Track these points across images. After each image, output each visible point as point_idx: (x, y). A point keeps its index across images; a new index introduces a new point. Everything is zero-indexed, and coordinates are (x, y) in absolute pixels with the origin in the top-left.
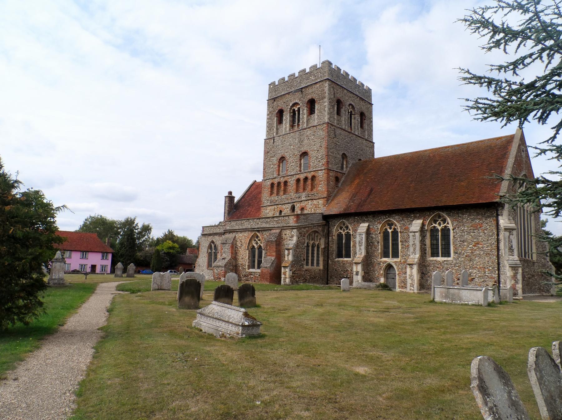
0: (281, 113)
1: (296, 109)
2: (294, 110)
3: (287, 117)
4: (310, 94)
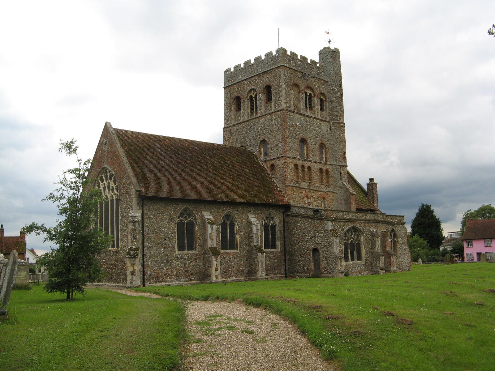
0: (238, 99)
1: (253, 96)
2: (251, 97)
3: (245, 104)
4: (268, 79)
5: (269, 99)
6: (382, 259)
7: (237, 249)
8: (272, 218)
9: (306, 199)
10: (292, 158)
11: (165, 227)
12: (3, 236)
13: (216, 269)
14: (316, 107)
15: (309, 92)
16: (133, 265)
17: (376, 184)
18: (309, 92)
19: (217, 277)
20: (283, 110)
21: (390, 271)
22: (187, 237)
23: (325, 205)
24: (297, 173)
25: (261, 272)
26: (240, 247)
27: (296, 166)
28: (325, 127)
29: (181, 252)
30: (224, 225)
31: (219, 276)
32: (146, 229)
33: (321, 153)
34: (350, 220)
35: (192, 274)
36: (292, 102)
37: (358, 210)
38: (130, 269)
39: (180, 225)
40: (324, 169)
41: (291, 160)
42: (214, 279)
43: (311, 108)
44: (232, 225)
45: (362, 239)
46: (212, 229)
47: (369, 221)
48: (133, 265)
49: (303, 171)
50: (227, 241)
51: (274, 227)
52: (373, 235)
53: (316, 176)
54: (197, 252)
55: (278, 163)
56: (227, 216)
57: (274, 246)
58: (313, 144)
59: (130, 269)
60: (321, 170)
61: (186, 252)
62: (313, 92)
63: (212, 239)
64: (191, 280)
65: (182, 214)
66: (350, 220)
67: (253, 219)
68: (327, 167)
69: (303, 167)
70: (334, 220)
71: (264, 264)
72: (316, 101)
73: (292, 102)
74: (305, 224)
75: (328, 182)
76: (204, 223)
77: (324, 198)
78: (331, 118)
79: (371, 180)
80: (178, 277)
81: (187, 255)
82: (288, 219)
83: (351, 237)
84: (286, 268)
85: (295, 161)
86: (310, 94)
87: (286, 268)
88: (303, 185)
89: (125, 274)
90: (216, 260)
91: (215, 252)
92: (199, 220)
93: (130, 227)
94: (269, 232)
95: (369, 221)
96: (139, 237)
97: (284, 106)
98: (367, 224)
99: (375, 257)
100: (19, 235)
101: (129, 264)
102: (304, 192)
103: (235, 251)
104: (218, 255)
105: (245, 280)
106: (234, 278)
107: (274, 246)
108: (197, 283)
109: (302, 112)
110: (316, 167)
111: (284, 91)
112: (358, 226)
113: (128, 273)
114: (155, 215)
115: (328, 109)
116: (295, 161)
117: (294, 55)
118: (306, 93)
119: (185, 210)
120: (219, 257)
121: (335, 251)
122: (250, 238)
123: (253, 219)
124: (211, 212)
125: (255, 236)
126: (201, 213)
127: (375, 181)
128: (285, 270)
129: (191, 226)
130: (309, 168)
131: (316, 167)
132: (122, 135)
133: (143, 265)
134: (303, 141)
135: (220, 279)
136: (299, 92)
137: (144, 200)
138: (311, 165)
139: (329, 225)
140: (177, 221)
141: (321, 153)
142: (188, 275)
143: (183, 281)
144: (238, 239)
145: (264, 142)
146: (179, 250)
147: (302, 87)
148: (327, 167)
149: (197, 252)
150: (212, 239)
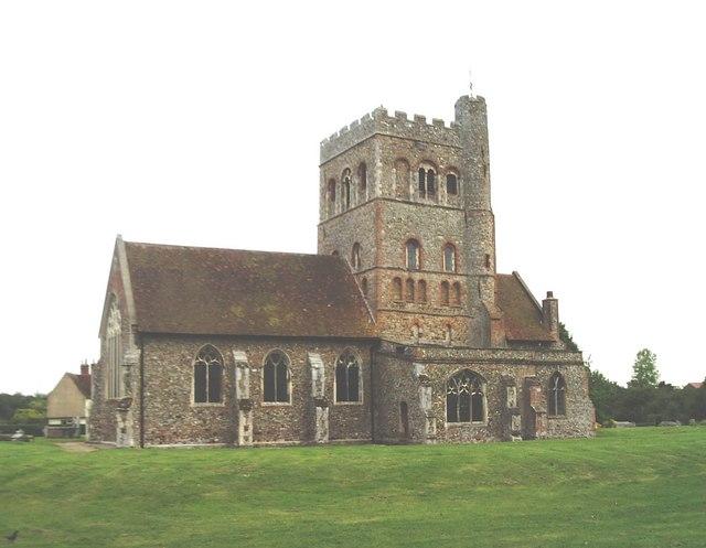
4: (363, 154)
5: (363, 185)
6: (517, 420)
7: (288, 401)
8: (352, 358)
9: (414, 329)
10: (389, 268)
11: (175, 371)
12: (488, 261)
13: (246, 429)
14: (440, 189)
15: (427, 168)
16: (124, 420)
17: (556, 300)
18: (427, 168)
19: (246, 439)
20: (377, 198)
21: (534, 438)
22: (212, 384)
23: (450, 335)
24: (400, 289)
25: (321, 434)
26: (295, 399)
27: (397, 280)
28: (455, 218)
29: (200, 404)
30: (268, 369)
31: (251, 438)
32: (147, 375)
33: (448, 257)
34: (460, 361)
35: (215, 434)
36: (394, 187)
37: (513, 344)
38: (121, 425)
39: (200, 369)
40: (451, 281)
41: (389, 272)
42: (242, 442)
43: (432, 191)
44: (283, 369)
45: (484, 388)
46: (243, 374)
47: (498, 361)
48: (124, 420)
49: (410, 289)
50: (274, 387)
51: (355, 369)
52: (507, 383)
53: (434, 294)
54: (223, 405)
55: (371, 275)
56: (275, 356)
57: (355, 398)
58: (431, 246)
59: (121, 425)
60: (445, 284)
61: (208, 404)
62: (436, 168)
63: (243, 388)
64: (214, 442)
65: (201, 355)
66: (460, 361)
67: (316, 360)
68: (458, 279)
69: (410, 281)
70: (424, 362)
71: (327, 423)
72: (441, 179)
73: (394, 187)
74: (395, 366)
75: (459, 302)
76: (233, 365)
77: (449, 326)
78: (467, 204)
79: (550, 294)
80: (193, 437)
81: (208, 408)
82: (379, 359)
83: (464, 387)
84: (373, 428)
85: (396, 274)
86: (430, 171)
87: (373, 428)
88: (409, 307)
89: (115, 430)
90: (247, 417)
91: (246, 405)
92: (226, 362)
93: (124, 371)
94: (346, 381)
95: (498, 361)
96: (135, 384)
97: (379, 193)
98: (494, 366)
99: (504, 415)
100: (449, 118)
101: (119, 419)
102: (410, 317)
103: (287, 404)
104: (249, 410)
105: (300, 445)
106: (282, 441)
107: (355, 398)
108: (223, 447)
109: (412, 200)
110: (435, 281)
111: (380, 172)
112: (476, 369)
113: (118, 431)
114: (160, 357)
115: (462, 191)
116: (396, 274)
117: (401, 116)
118: (422, 171)
119: (207, 348)
120: (250, 413)
121: (424, 406)
122: (307, 385)
123: (316, 360)
124: (247, 351)
125: (314, 383)
126: (231, 352)
127: (555, 296)
128: (372, 432)
129: (216, 369)
130: (422, 282)
131: (435, 281)
132: (129, 247)
133: (142, 421)
134: (413, 243)
135: (250, 443)
136: (409, 170)
137: (143, 338)
138: (426, 277)
139: (420, 369)
140: (193, 364)
141: (448, 257)
142: (209, 435)
143: (201, 443)
144: (291, 387)
145: (357, 246)
146: (196, 401)
147: (413, 161)
148: (458, 279)
149: (223, 405)
150: (243, 388)
